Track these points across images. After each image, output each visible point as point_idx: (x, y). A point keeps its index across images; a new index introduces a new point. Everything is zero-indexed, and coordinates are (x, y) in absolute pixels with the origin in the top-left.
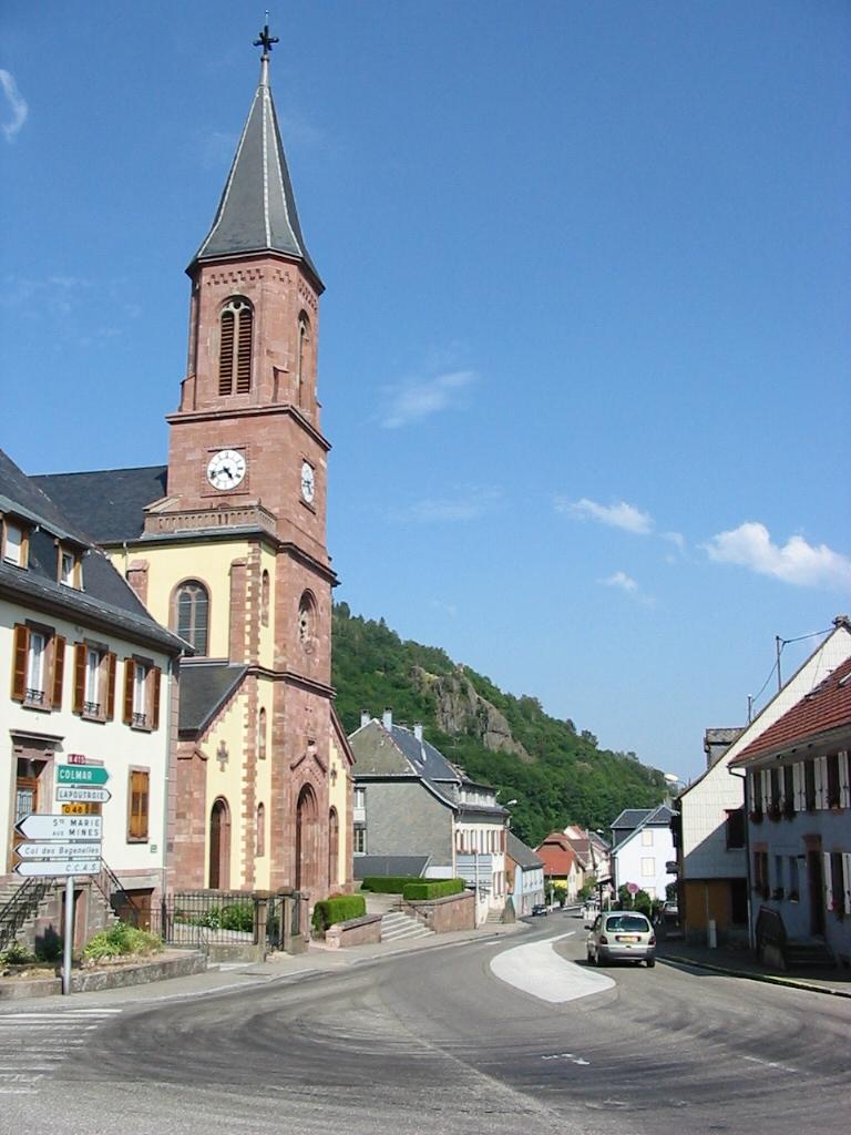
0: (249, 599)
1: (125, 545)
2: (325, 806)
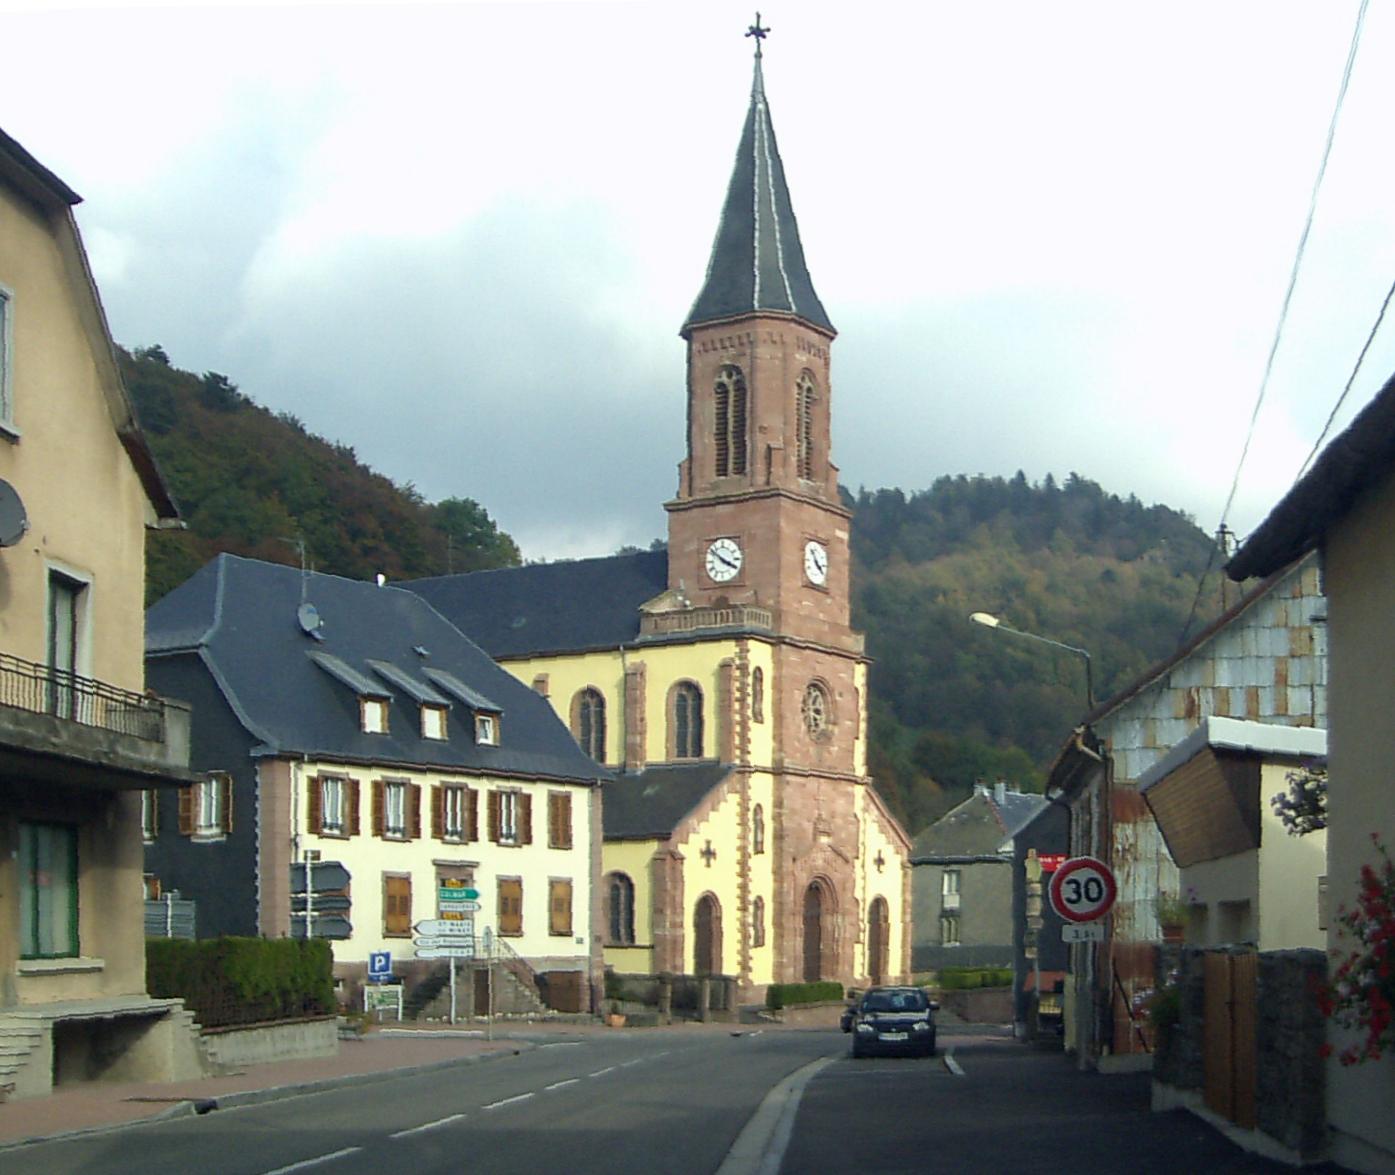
0: (737, 700)
1: (621, 648)
2: (850, 895)
